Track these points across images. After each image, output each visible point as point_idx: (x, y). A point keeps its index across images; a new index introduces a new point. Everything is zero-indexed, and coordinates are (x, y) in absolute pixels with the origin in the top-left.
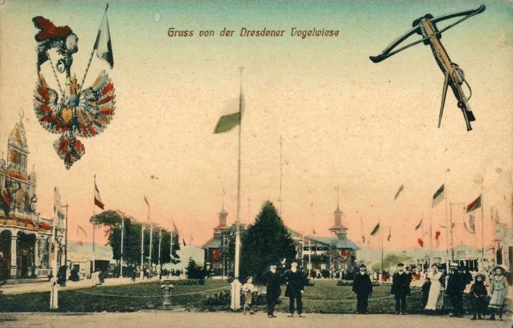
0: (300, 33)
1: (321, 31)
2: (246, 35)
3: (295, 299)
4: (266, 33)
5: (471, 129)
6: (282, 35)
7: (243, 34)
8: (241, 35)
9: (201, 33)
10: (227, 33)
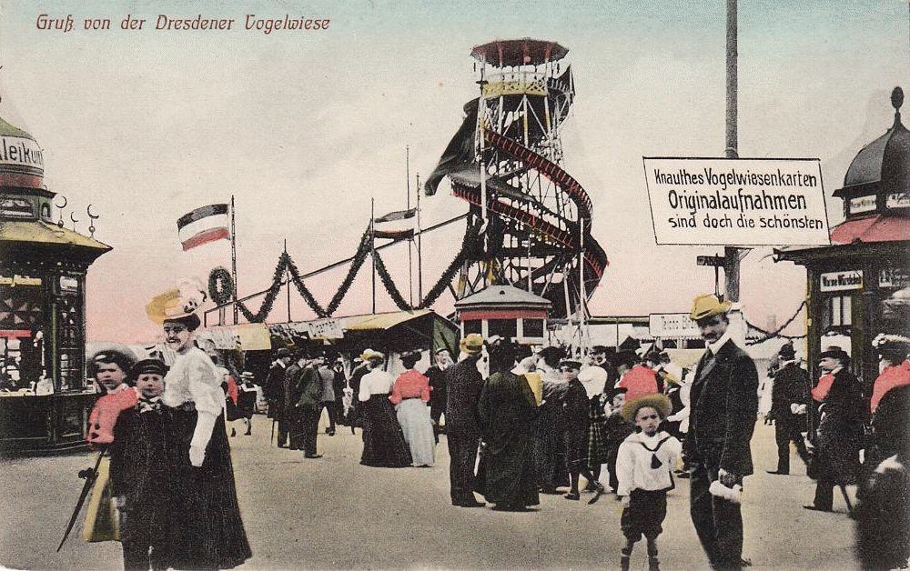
0: (260, 23)
1: (297, 21)
2: (167, 26)
3: (38, 281)
4: (200, 24)
5: (786, 472)
6: (229, 28)
7: (161, 26)
8: (157, 28)
9: (88, 24)
10: (128, 24)
